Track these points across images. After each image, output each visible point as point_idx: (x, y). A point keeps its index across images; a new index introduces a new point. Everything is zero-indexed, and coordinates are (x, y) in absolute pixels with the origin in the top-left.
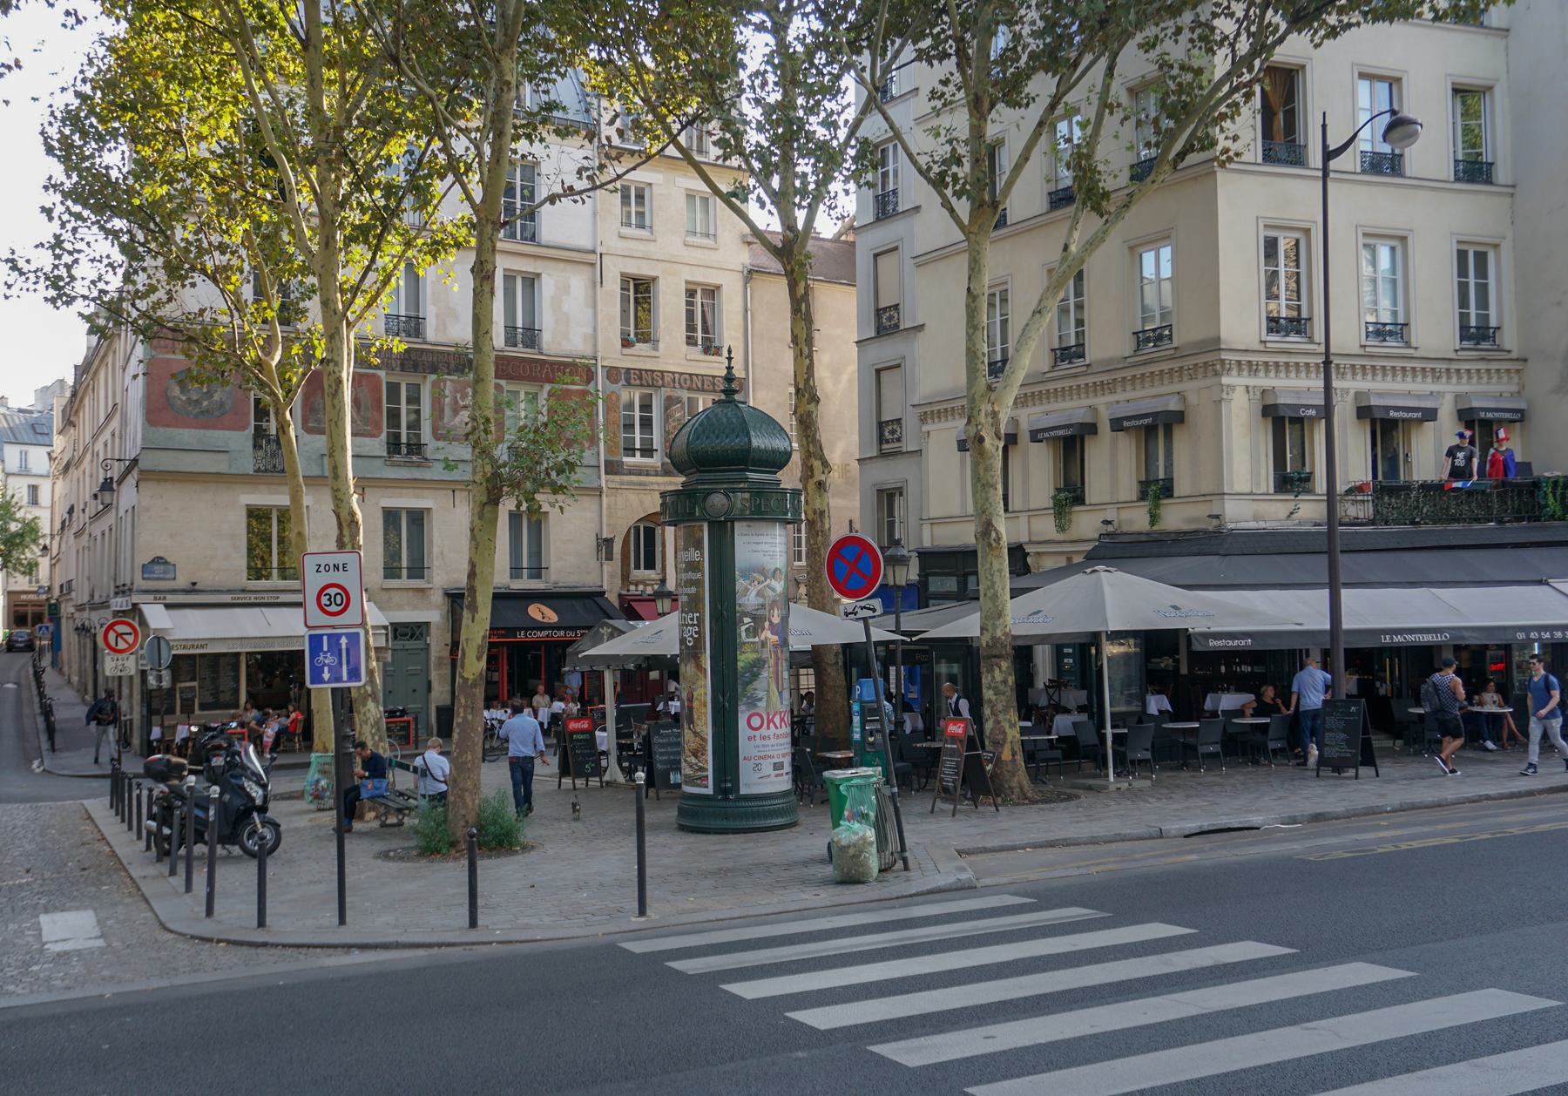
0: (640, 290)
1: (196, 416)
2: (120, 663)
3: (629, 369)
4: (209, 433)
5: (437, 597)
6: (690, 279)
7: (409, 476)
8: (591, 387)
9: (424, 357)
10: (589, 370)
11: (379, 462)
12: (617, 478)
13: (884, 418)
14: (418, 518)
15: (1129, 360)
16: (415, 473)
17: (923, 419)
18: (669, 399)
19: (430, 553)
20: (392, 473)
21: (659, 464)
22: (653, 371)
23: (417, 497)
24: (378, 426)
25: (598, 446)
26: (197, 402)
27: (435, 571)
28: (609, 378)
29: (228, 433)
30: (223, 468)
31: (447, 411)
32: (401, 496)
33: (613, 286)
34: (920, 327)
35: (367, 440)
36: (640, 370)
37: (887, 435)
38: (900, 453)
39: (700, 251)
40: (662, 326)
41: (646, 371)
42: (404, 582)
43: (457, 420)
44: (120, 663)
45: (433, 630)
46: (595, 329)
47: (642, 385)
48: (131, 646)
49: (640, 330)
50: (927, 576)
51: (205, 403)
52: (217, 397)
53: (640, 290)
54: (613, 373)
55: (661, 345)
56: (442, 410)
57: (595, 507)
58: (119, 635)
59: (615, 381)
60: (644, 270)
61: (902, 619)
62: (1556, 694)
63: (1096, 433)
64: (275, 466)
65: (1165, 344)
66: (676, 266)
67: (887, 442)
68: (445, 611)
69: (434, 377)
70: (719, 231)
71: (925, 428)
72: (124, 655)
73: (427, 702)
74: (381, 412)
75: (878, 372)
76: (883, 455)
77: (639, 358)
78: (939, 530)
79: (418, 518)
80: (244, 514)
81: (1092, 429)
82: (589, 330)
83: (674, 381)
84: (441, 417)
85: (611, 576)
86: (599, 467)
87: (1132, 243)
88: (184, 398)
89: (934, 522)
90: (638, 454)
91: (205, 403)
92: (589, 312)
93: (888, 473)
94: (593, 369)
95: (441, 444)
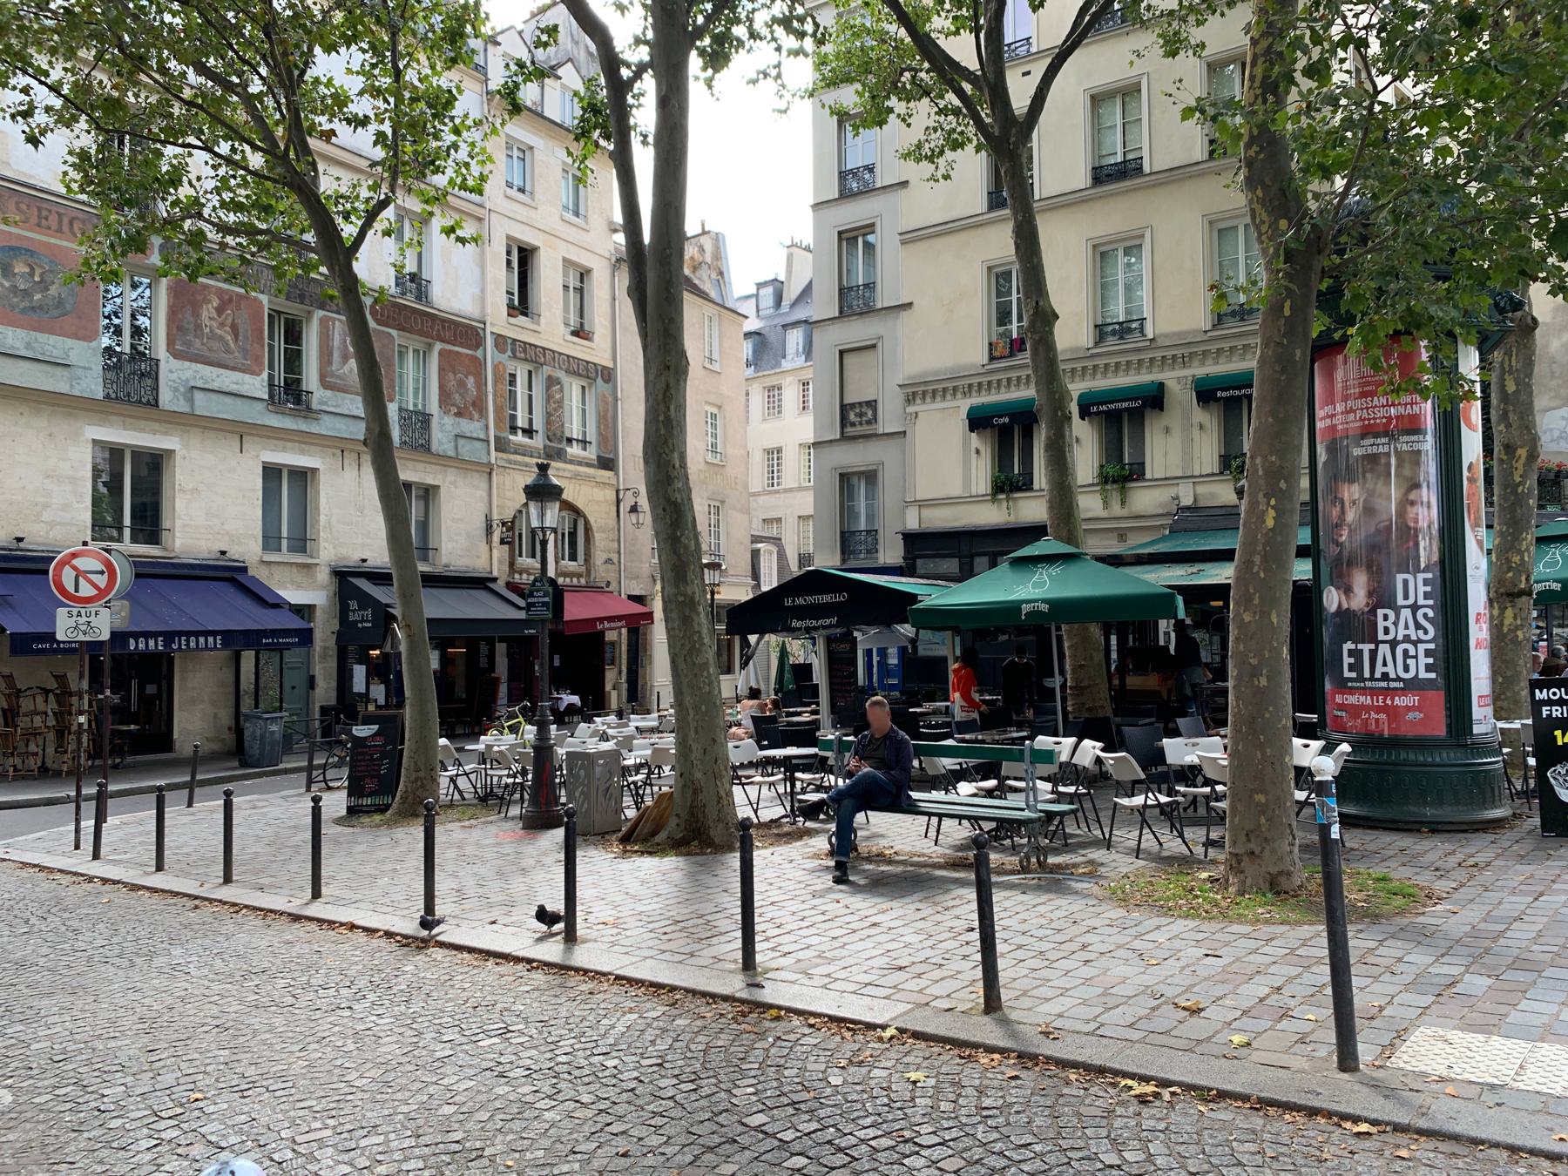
0: (524, 258)
1: (23, 311)
2: (83, 620)
3: (515, 340)
4: (42, 337)
5: (323, 575)
6: (567, 256)
7: (294, 427)
8: (479, 353)
9: (311, 288)
10: (478, 334)
11: (260, 406)
12: (504, 456)
13: (848, 400)
14: (303, 478)
15: (1210, 334)
16: (302, 425)
17: (910, 399)
18: (550, 378)
19: (318, 521)
20: (275, 421)
21: (541, 447)
22: (536, 346)
23: (302, 452)
24: (258, 359)
25: (487, 419)
26: (26, 293)
27: (322, 544)
28: (496, 346)
29: (70, 342)
30: (63, 387)
31: (336, 355)
32: (284, 449)
33: (498, 249)
34: (910, 305)
35: (247, 377)
36: (525, 343)
37: (852, 417)
38: (876, 435)
39: (574, 229)
40: (543, 300)
41: (530, 345)
42: (285, 556)
43: (346, 368)
44: (83, 620)
45: (318, 613)
46: (483, 291)
47: (526, 360)
48: (102, 593)
49: (522, 304)
50: (914, 559)
51: (37, 297)
52: (53, 290)
53: (524, 258)
54: (500, 340)
55: (542, 320)
56: (330, 354)
57: (484, 485)
58: (79, 574)
59: (503, 351)
60: (529, 237)
61: (286, 660)
62: (875, 698)
63: (1162, 409)
64: (129, 395)
65: (1133, 341)
66: (558, 241)
67: (853, 424)
68: (331, 594)
69: (321, 313)
70: (590, 212)
71: (910, 409)
72: (92, 608)
73: (308, 701)
74: (263, 346)
75: (841, 353)
76: (844, 437)
77: (518, 329)
78: (927, 513)
79: (303, 478)
80: (90, 446)
81: (1154, 399)
82: (477, 291)
83: (554, 359)
84: (330, 363)
85: (500, 562)
86: (488, 441)
87: (1097, 241)
88: (7, 284)
89: (922, 504)
90: (520, 432)
91: (37, 297)
92: (477, 270)
93: (855, 457)
94: (481, 332)
95: (329, 393)
